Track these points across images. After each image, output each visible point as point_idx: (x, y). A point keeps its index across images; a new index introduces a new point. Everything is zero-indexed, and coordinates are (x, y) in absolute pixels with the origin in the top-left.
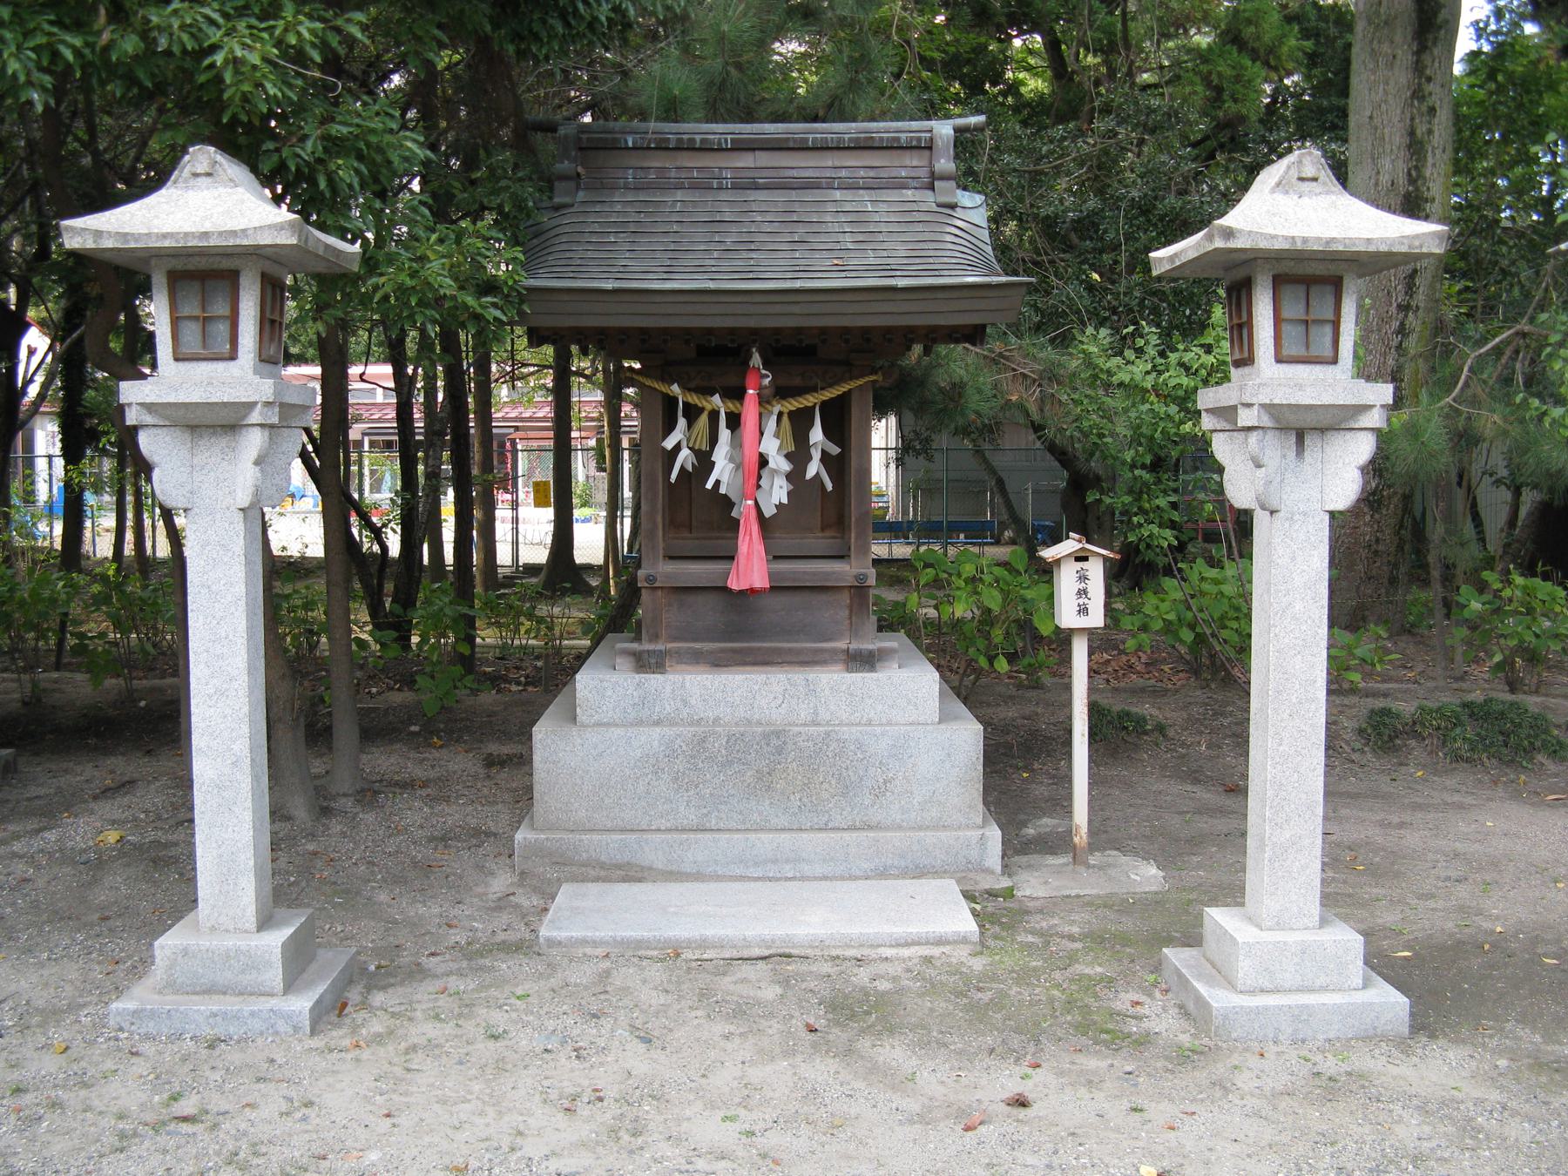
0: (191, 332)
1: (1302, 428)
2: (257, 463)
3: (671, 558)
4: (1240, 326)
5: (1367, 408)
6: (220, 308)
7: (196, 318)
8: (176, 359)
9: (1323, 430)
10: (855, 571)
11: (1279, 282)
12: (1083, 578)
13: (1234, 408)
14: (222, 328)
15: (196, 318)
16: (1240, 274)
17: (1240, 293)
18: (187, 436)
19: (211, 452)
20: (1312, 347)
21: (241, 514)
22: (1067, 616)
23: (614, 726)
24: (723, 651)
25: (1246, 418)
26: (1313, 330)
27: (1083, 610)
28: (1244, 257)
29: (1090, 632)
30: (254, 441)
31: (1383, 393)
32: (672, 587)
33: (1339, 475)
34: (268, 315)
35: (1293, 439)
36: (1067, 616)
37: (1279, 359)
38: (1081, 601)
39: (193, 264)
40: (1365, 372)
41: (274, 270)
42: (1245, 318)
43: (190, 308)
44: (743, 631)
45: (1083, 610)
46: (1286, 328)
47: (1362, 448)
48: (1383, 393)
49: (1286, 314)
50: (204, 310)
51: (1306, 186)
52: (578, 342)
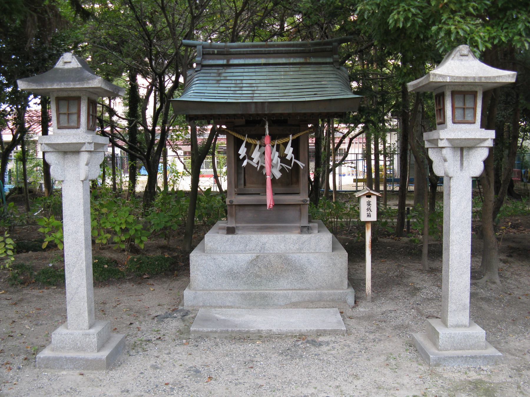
0: (459, 113)
1: (463, 148)
2: (87, 164)
3: (238, 194)
4: (440, 110)
5: (485, 140)
6: (74, 110)
7: (65, 114)
8: (58, 128)
9: (470, 148)
10: (302, 199)
11: (454, 94)
12: (369, 204)
13: (437, 140)
14: (75, 117)
15: (65, 114)
16: (440, 91)
17: (440, 98)
18: (60, 156)
19: (71, 159)
20: (466, 117)
21: (81, 182)
22: (364, 218)
23: (218, 255)
24: (261, 226)
25: (441, 144)
26: (71, 116)
27: (369, 216)
28: (437, 85)
29: (373, 223)
30: (84, 157)
31: (491, 134)
32: (240, 206)
33: (476, 163)
34: (91, 113)
35: (459, 152)
36: (364, 218)
37: (454, 123)
38: (368, 212)
39: (65, 94)
40: (486, 125)
41: (93, 97)
42: (442, 107)
43: (63, 110)
44: (269, 219)
45: (369, 216)
46: (62, 117)
47: (484, 154)
48: (491, 134)
49: (456, 105)
50: (68, 109)
51: (464, 58)
52: (320, 118)
